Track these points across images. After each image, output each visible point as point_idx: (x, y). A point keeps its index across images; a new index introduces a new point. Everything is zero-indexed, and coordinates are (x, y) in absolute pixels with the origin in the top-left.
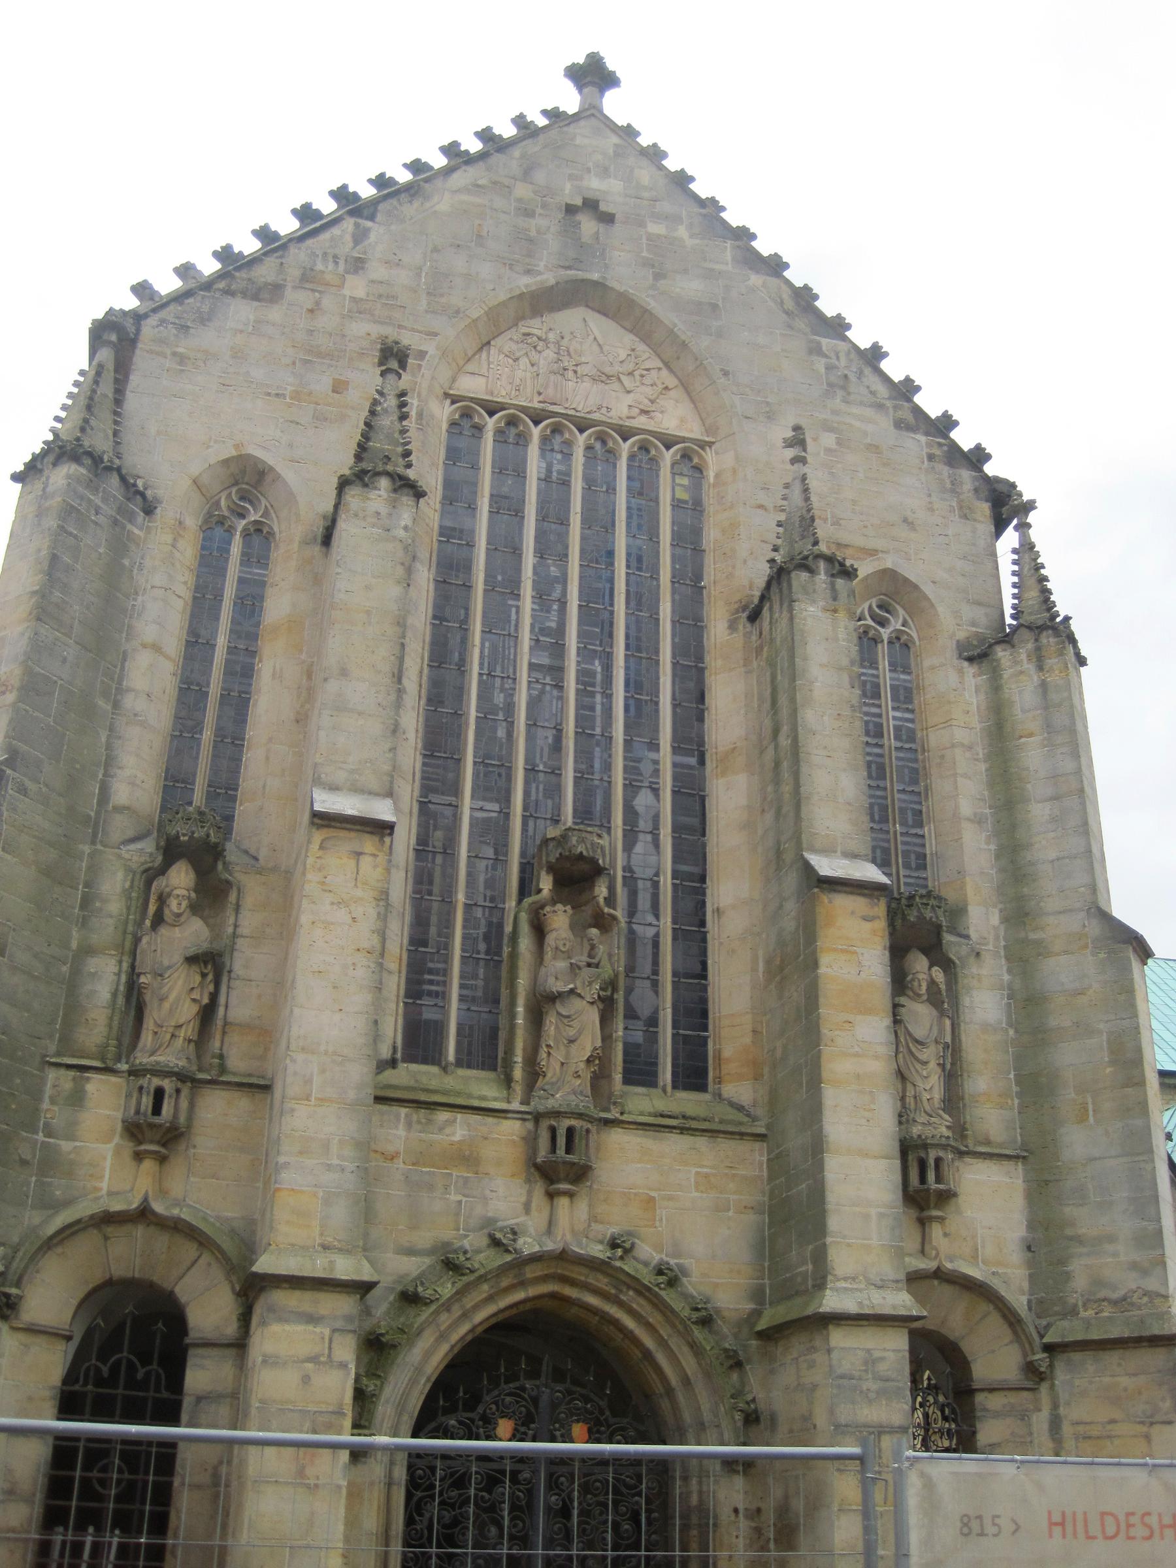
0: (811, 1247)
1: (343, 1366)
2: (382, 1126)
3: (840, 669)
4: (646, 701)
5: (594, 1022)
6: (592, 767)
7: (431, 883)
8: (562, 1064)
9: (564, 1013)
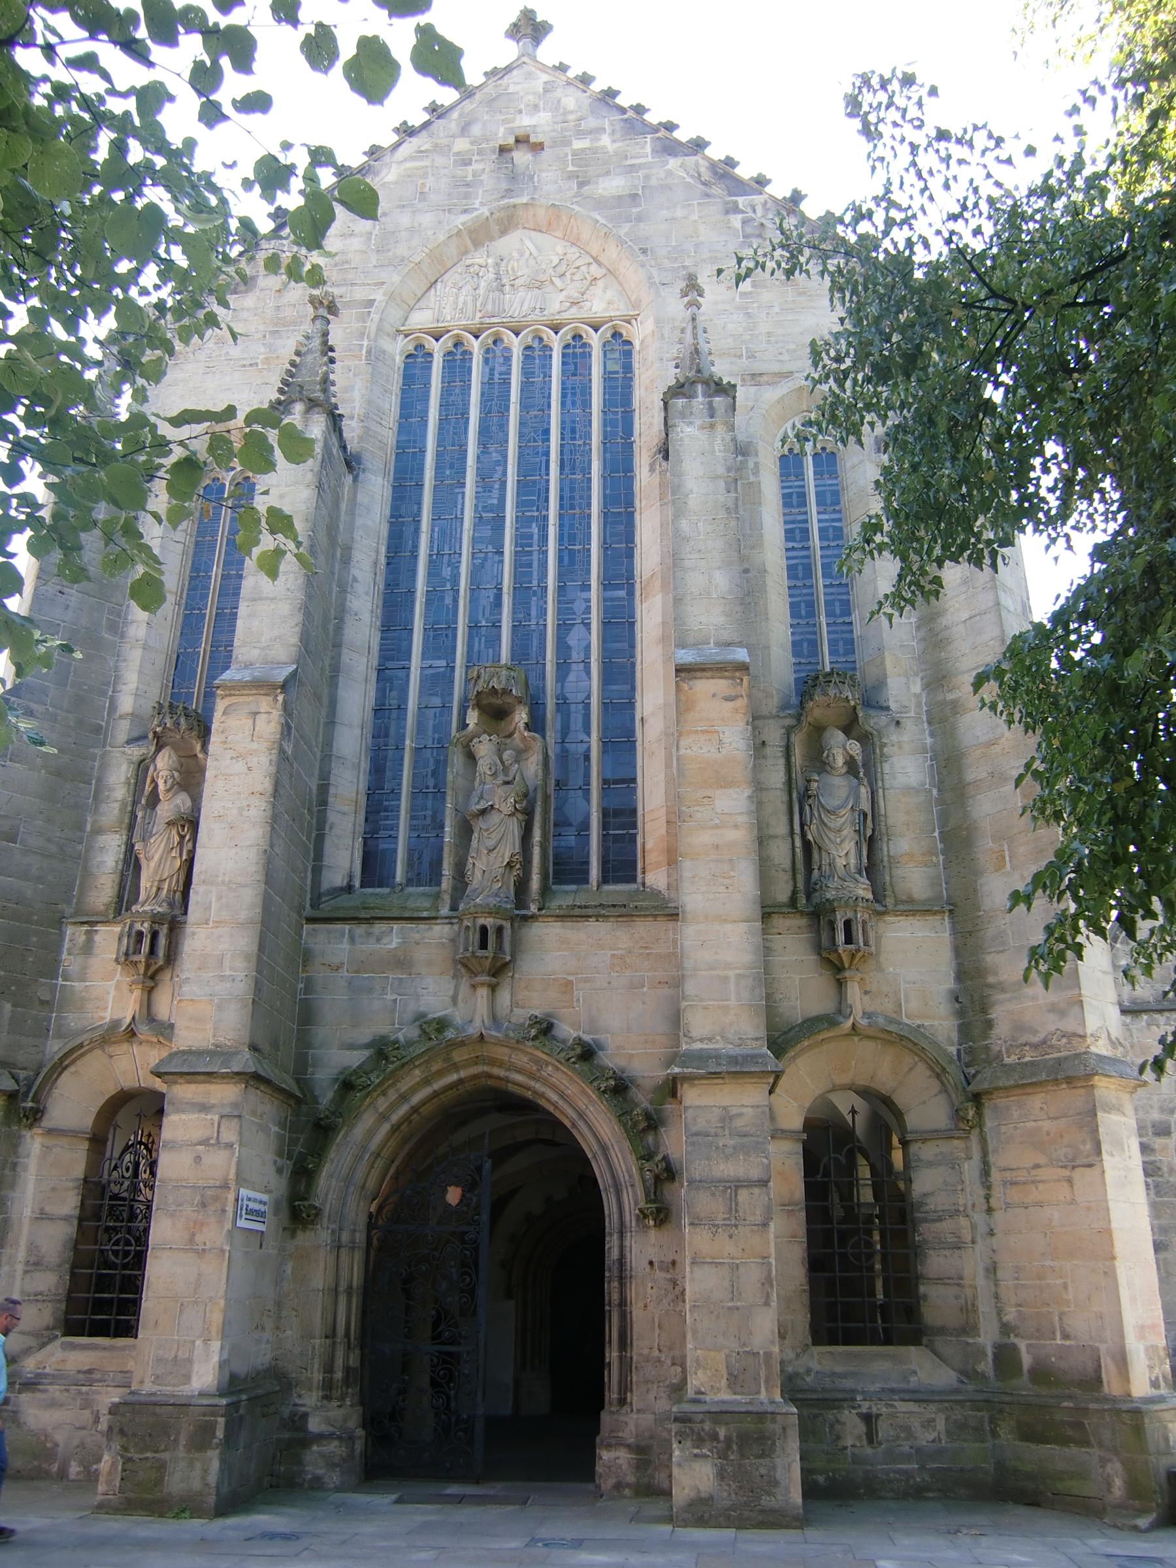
1: (230, 1146)
2: (329, 942)
3: (717, 477)
4: (579, 551)
6: (529, 615)
7: (387, 736)
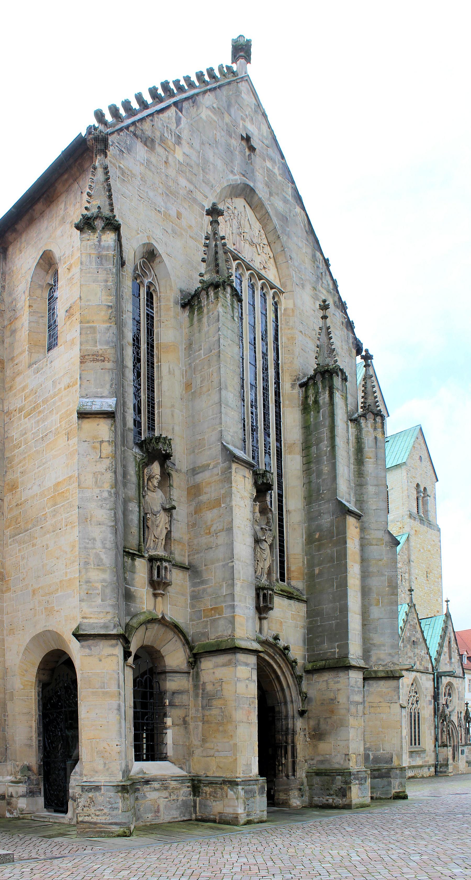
0: (337, 644)
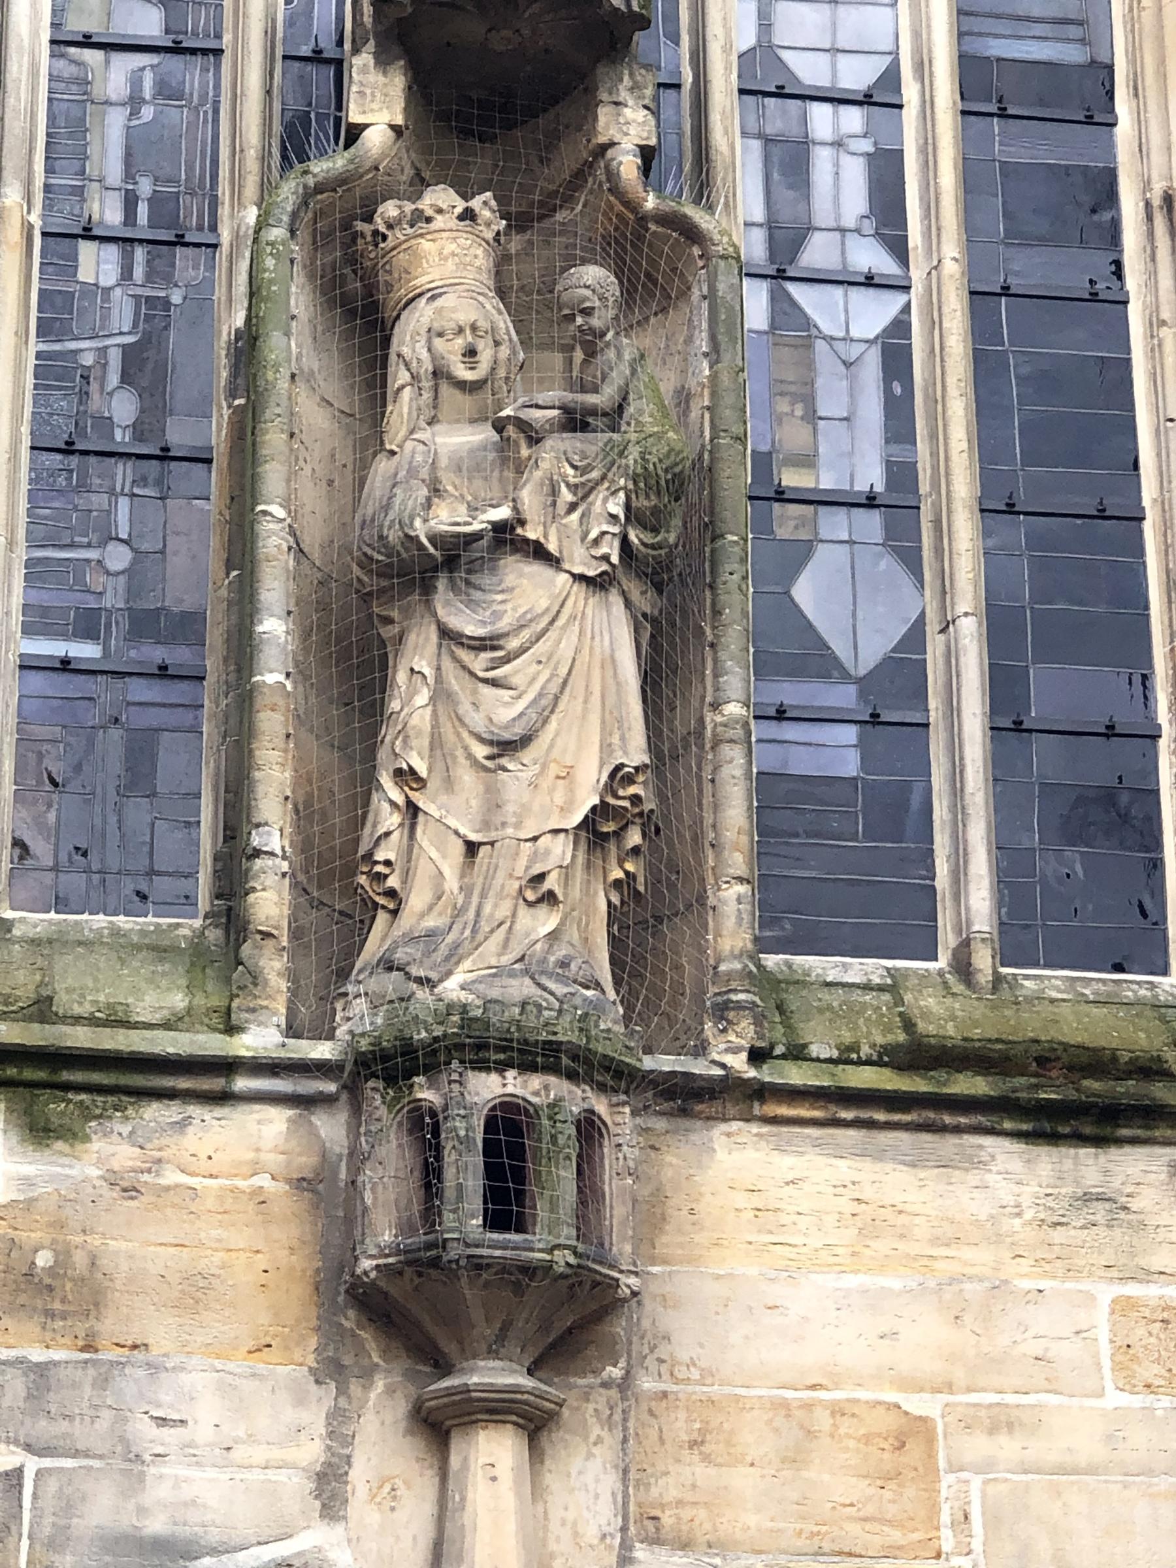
5: (612, 661)
8: (472, 848)
9: (470, 630)
